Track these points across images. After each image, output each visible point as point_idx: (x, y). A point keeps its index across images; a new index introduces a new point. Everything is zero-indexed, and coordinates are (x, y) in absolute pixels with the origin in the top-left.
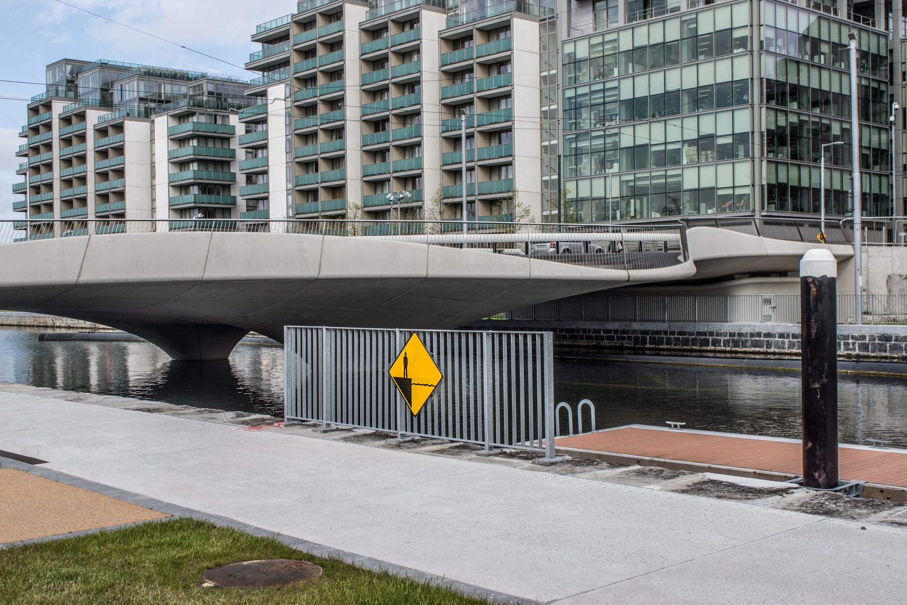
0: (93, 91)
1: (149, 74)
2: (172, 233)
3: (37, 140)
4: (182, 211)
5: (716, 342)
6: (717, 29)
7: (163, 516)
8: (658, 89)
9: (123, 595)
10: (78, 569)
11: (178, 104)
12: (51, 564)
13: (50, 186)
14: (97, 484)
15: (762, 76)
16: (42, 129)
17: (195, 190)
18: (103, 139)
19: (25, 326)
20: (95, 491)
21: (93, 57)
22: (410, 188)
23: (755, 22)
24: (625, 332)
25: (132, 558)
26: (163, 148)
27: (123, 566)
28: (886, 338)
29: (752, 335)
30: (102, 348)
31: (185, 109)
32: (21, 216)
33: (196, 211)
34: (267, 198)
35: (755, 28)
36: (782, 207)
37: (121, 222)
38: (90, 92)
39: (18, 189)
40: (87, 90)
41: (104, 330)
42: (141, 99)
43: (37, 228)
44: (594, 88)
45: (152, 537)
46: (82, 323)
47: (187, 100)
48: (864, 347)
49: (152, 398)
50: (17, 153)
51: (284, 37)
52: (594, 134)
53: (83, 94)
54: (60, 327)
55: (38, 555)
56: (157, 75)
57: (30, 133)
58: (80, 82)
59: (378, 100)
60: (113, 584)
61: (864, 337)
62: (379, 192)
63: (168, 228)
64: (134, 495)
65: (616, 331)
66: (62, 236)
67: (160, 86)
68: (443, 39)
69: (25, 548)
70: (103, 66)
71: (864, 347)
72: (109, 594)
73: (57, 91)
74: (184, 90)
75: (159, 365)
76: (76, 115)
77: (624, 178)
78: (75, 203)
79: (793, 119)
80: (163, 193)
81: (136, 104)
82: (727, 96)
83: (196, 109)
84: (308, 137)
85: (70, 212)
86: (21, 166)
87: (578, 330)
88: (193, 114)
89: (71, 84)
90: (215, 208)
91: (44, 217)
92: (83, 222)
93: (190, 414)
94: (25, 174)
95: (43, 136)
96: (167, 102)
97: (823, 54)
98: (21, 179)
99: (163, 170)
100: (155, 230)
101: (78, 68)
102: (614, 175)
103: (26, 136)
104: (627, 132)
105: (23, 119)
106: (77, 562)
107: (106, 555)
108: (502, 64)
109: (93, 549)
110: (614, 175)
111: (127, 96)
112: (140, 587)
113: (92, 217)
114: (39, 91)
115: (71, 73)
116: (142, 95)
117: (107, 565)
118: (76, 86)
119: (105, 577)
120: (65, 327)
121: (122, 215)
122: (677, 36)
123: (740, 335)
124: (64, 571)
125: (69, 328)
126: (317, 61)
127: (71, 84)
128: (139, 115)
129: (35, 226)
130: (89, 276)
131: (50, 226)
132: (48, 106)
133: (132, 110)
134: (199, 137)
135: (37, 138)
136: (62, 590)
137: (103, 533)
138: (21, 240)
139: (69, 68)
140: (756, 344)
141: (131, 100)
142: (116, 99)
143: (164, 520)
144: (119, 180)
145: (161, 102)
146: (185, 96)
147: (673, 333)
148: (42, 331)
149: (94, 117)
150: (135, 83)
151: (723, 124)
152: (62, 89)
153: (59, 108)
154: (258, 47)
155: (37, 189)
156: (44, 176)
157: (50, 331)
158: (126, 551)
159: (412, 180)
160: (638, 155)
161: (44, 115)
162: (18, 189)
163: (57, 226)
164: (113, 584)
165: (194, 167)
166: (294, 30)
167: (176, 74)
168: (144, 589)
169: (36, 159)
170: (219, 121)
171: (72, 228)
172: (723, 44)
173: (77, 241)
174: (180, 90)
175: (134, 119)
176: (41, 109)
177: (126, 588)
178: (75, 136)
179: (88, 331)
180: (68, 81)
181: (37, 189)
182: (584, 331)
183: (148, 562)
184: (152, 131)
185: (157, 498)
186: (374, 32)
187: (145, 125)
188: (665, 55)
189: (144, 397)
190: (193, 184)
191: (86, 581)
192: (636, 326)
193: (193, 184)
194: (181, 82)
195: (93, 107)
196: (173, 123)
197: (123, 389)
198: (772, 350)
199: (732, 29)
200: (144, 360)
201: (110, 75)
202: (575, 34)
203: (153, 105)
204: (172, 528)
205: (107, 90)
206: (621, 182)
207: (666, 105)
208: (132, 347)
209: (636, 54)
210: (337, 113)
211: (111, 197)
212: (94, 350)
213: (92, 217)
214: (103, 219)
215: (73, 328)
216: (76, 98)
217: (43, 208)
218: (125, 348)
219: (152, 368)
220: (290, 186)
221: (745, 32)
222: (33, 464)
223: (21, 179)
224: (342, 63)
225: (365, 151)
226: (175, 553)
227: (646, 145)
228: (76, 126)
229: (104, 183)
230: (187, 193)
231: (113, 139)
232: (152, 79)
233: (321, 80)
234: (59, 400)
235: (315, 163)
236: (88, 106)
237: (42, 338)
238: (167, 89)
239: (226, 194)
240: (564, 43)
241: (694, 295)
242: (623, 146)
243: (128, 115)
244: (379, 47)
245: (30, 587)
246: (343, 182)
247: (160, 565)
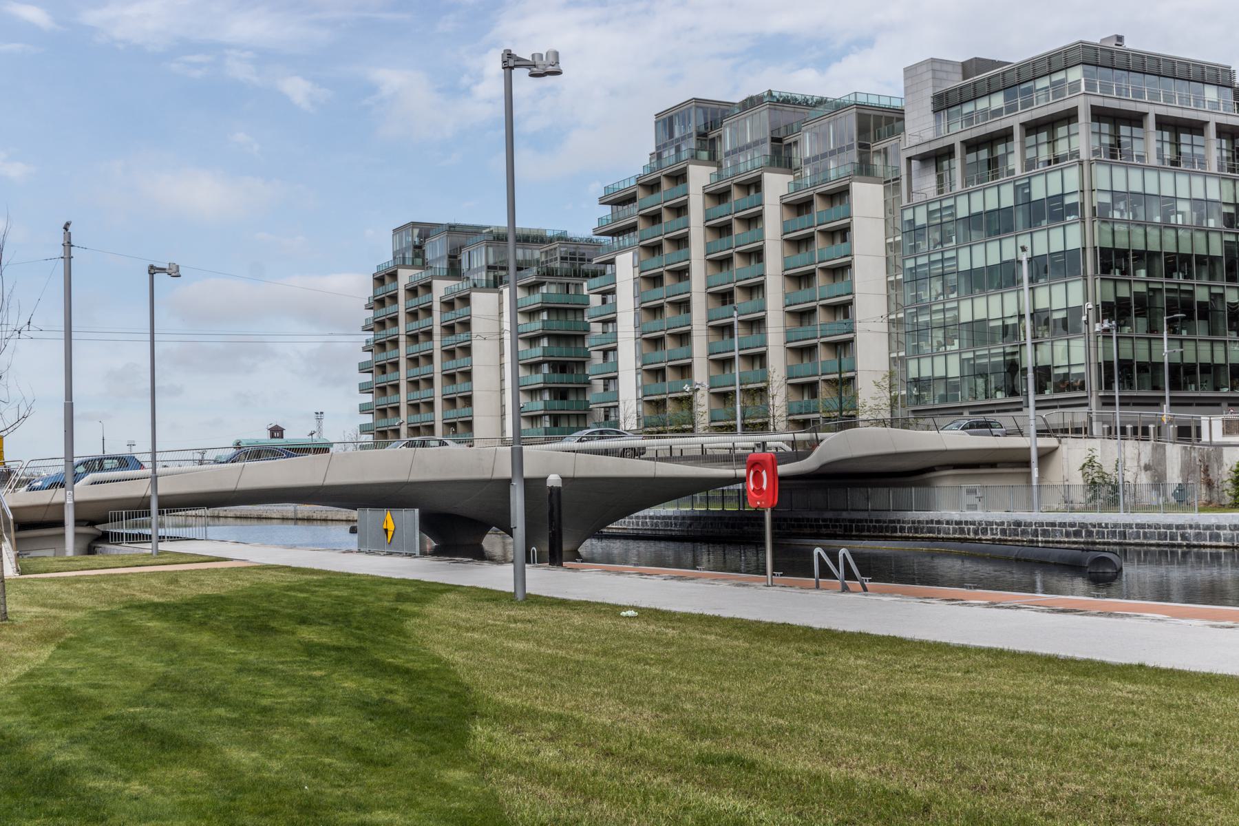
3: (383, 313)
5: (902, 530)
6: (1050, 194)
8: (994, 260)
13: (429, 358)
15: (1097, 244)
17: (545, 369)
22: (757, 367)
23: (1086, 188)
24: (837, 520)
28: (1018, 524)
29: (927, 522)
34: (615, 378)
35: (1087, 194)
36: (1131, 386)
39: (364, 368)
42: (489, 268)
44: (934, 258)
48: (1003, 532)
51: (630, 199)
52: (934, 308)
59: (803, 251)
61: (1002, 523)
62: (727, 372)
65: (831, 520)
70: (452, 229)
71: (1003, 532)
73: (404, 258)
76: (423, 286)
77: (965, 356)
79: (1141, 288)
81: (484, 274)
82: (1048, 268)
84: (656, 311)
87: (803, 519)
88: (543, 284)
89: (419, 249)
90: (568, 388)
97: (1182, 213)
101: (426, 231)
102: (953, 353)
104: (965, 306)
105: (366, 290)
108: (843, 233)
110: (953, 353)
111: (475, 265)
114: (385, 257)
115: (419, 236)
116: (491, 262)
122: (1011, 203)
123: (919, 522)
126: (662, 227)
127: (419, 249)
128: (487, 286)
132: (394, 276)
134: (549, 310)
135: (382, 312)
139: (416, 231)
140: (930, 530)
142: (465, 266)
147: (871, 521)
149: (441, 288)
150: (484, 250)
151: (1062, 296)
152: (409, 255)
153: (406, 277)
154: (607, 210)
156: (390, 354)
159: (759, 359)
160: (978, 331)
161: (389, 286)
165: (545, 342)
166: (641, 194)
170: (572, 291)
172: (1055, 210)
175: (482, 290)
180: (416, 247)
182: (808, 520)
186: (719, 196)
187: (493, 297)
188: (995, 224)
190: (544, 362)
192: (845, 515)
193: (544, 362)
194: (534, 246)
196: (521, 294)
198: (942, 535)
199: (1063, 195)
201: (787, 116)
202: (916, 199)
206: (962, 361)
207: (1002, 277)
209: (973, 221)
210: (682, 285)
216: (424, 265)
220: (639, 364)
221: (1075, 199)
223: (368, 357)
224: (760, 208)
225: (789, 312)
227: (984, 320)
228: (422, 299)
230: (537, 373)
231: (460, 311)
233: (667, 248)
235: (730, 327)
239: (580, 372)
240: (903, 209)
241: (866, 486)
242: (962, 321)
243: (475, 286)
244: (724, 213)
246: (851, 336)
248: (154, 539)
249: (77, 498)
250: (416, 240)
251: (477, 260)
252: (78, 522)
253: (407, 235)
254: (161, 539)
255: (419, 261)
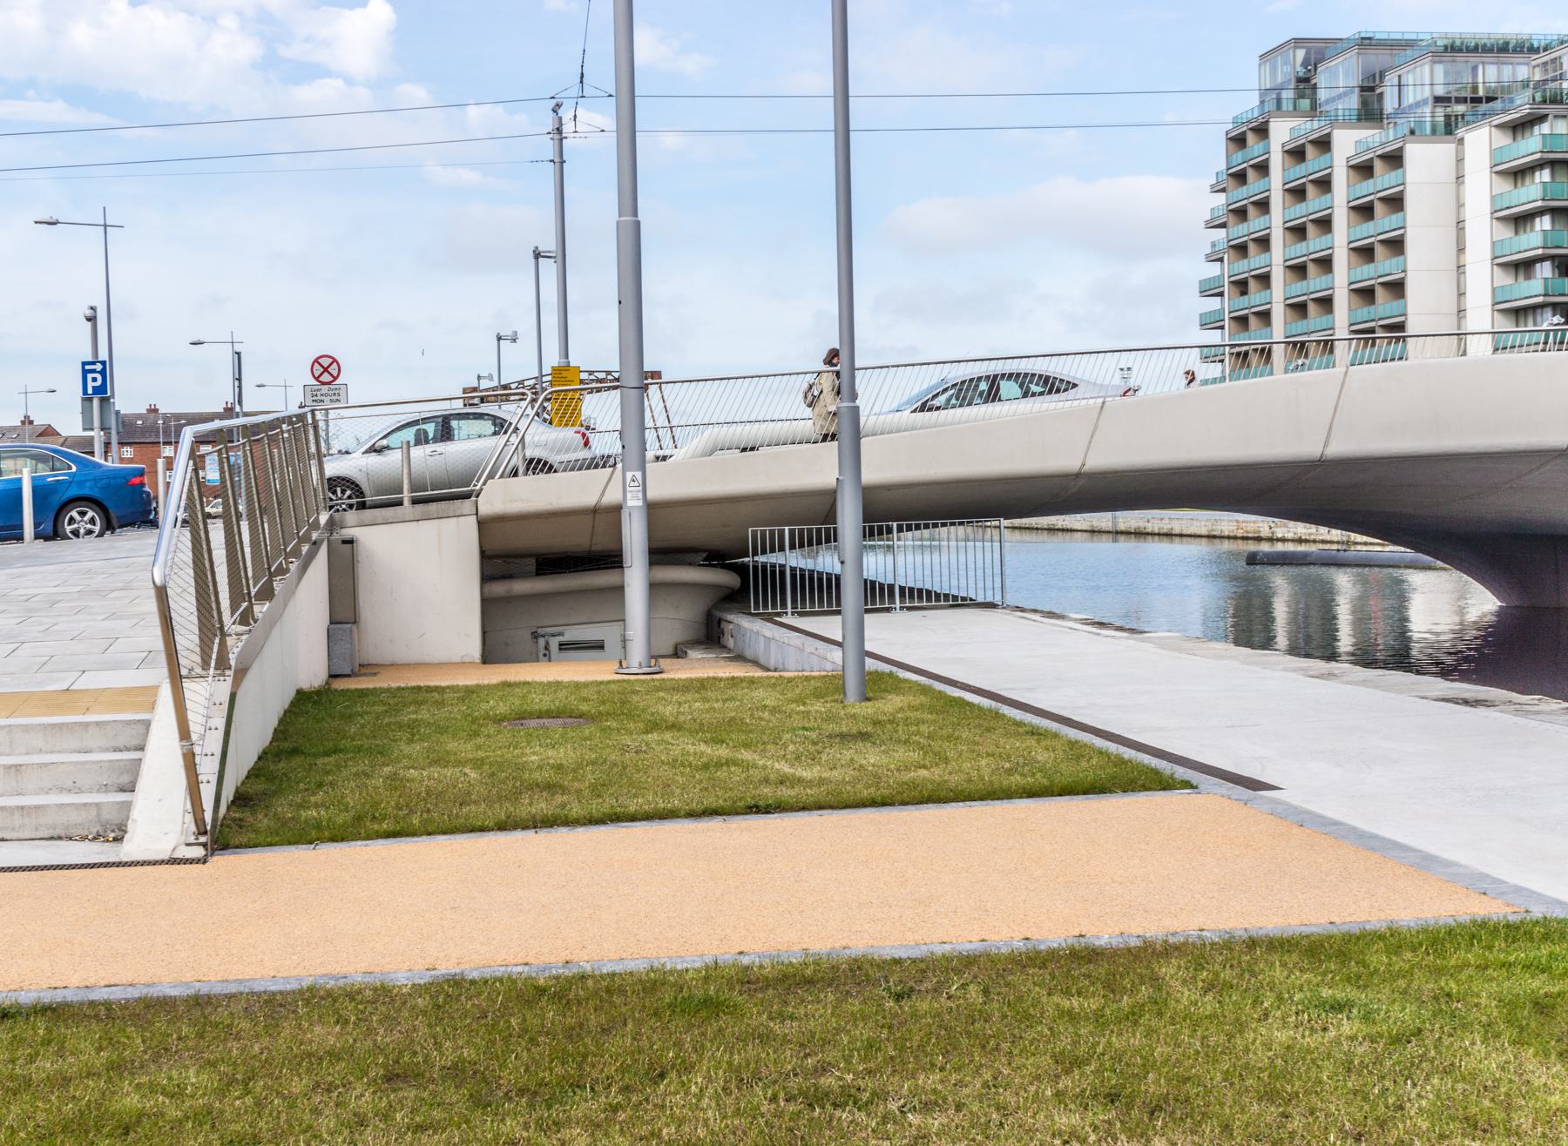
0: (1345, 94)
1: (1453, 49)
2: (1500, 356)
3: (1243, 194)
4: (1519, 313)
7: (1510, 910)
9: (1440, 1053)
10: (1351, 993)
11: (1511, 101)
12: (1299, 978)
14: (1376, 837)
16: (1251, 174)
17: (1545, 270)
18: (1365, 184)
19: (1222, 537)
20: (1373, 849)
21: (1345, 31)
25: (1453, 985)
26: (1481, 190)
27: (1436, 998)
30: (1364, 581)
31: (1526, 110)
32: (1214, 337)
33: (1548, 312)
37: (1398, 339)
38: (1340, 97)
39: (1210, 290)
40: (1334, 93)
41: (1365, 545)
42: (1438, 100)
43: (1242, 358)
45: (1490, 948)
46: (1323, 532)
47: (1529, 93)
49: (1465, 677)
50: (1207, 222)
53: (1328, 102)
54: (1283, 540)
55: (1276, 957)
56: (1468, 50)
57: (1231, 183)
58: (1321, 79)
60: (1420, 1031)
63: (1490, 349)
64: (1448, 864)
66: (1286, 371)
67: (1475, 69)
68: (1352, 167)
69: (1252, 943)
70: (1365, 43)
72: (1413, 1049)
73: (1279, 100)
74: (1523, 72)
75: (1473, 615)
78: (1312, 308)
80: (1482, 280)
81: (1428, 110)
83: (1550, 109)
85: (1302, 326)
86: (1213, 245)
88: (1542, 119)
91: (1255, 337)
92: (1326, 342)
93: (1551, 713)
94: (1221, 260)
95: (1254, 187)
96: (1490, 99)
98: (1214, 270)
99: (1482, 234)
100: (1464, 354)
101: (1317, 52)
103: (1223, 190)
105: (1217, 159)
106: (1348, 980)
107: (1402, 974)
109: (1378, 959)
111: (1410, 97)
112: (1473, 1044)
113: (1341, 331)
114: (1247, 105)
115: (1305, 63)
116: (1440, 91)
117: (1405, 992)
118: (1315, 87)
119: (1404, 1015)
120: (1293, 540)
121: (1400, 327)
124: (1326, 993)
125: (1300, 541)
127: (1305, 84)
128: (1434, 132)
129: (1238, 354)
130: (1343, 446)
131: (1266, 353)
132: (1262, 131)
133: (1421, 123)
135: (1243, 192)
136: (1325, 1029)
137: (1393, 932)
138: (1214, 381)
139: (1301, 54)
141: (1418, 105)
142: (1390, 104)
143: (1511, 918)
144: (1395, 260)
145: (1476, 100)
146: (1525, 84)
148: (1252, 547)
149: (1349, 143)
150: (1427, 69)
152: (1288, 95)
153: (1283, 132)
155: (1242, 286)
157: (1265, 547)
158: (1438, 972)
161: (1254, 147)
162: (1210, 290)
163: (1278, 351)
164: (1420, 1031)
165: (1545, 223)
167: (1507, 43)
168: (1480, 1048)
169: (1241, 231)
171: (1306, 356)
173: (1317, 380)
174: (1514, 73)
175: (1424, 139)
176: (1251, 138)
177: (1446, 1041)
178: (1312, 181)
179: (1335, 547)
180: (1299, 80)
181: (1242, 286)
183: (1486, 994)
184: (1460, 161)
185: (1495, 874)
187: (1442, 151)
189: (1445, 672)
190: (1541, 259)
191: (1367, 1018)
193: (1541, 259)
194: (1519, 58)
195: (1346, 124)
196: (1502, 139)
197: (1400, 658)
200: (1446, 602)
201: (1378, 59)
203: (1460, 108)
204: (1529, 935)
205: (1372, 89)
208: (1416, 578)
211: (1379, 292)
212: (1344, 583)
213: (1341, 331)
214: (1364, 335)
215: (1307, 541)
216: (1314, 110)
217: (1253, 321)
218: (1400, 582)
219: (1457, 619)
222: (1255, 790)
226: (1538, 984)
228: (1314, 164)
229: (1366, 267)
230: (1528, 277)
231: (1384, 180)
232: (1460, 58)
234: (1294, 675)
236: (1335, 122)
237: (1252, 559)
238: (1490, 74)
243: (1412, 132)
245: (1266, 1015)
247: (1510, 1005)
248: (851, 595)
249: (655, 493)
250: (1299, 68)
251: (1420, 83)
252: (660, 554)
253: (1285, 63)
254: (878, 595)
255: (1305, 104)
